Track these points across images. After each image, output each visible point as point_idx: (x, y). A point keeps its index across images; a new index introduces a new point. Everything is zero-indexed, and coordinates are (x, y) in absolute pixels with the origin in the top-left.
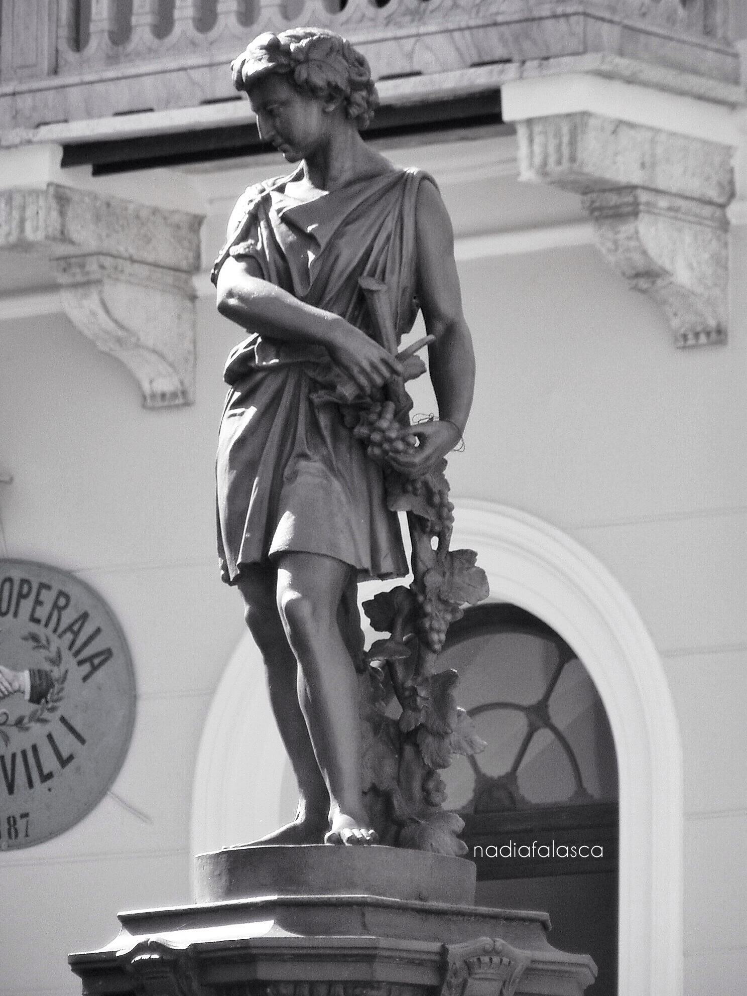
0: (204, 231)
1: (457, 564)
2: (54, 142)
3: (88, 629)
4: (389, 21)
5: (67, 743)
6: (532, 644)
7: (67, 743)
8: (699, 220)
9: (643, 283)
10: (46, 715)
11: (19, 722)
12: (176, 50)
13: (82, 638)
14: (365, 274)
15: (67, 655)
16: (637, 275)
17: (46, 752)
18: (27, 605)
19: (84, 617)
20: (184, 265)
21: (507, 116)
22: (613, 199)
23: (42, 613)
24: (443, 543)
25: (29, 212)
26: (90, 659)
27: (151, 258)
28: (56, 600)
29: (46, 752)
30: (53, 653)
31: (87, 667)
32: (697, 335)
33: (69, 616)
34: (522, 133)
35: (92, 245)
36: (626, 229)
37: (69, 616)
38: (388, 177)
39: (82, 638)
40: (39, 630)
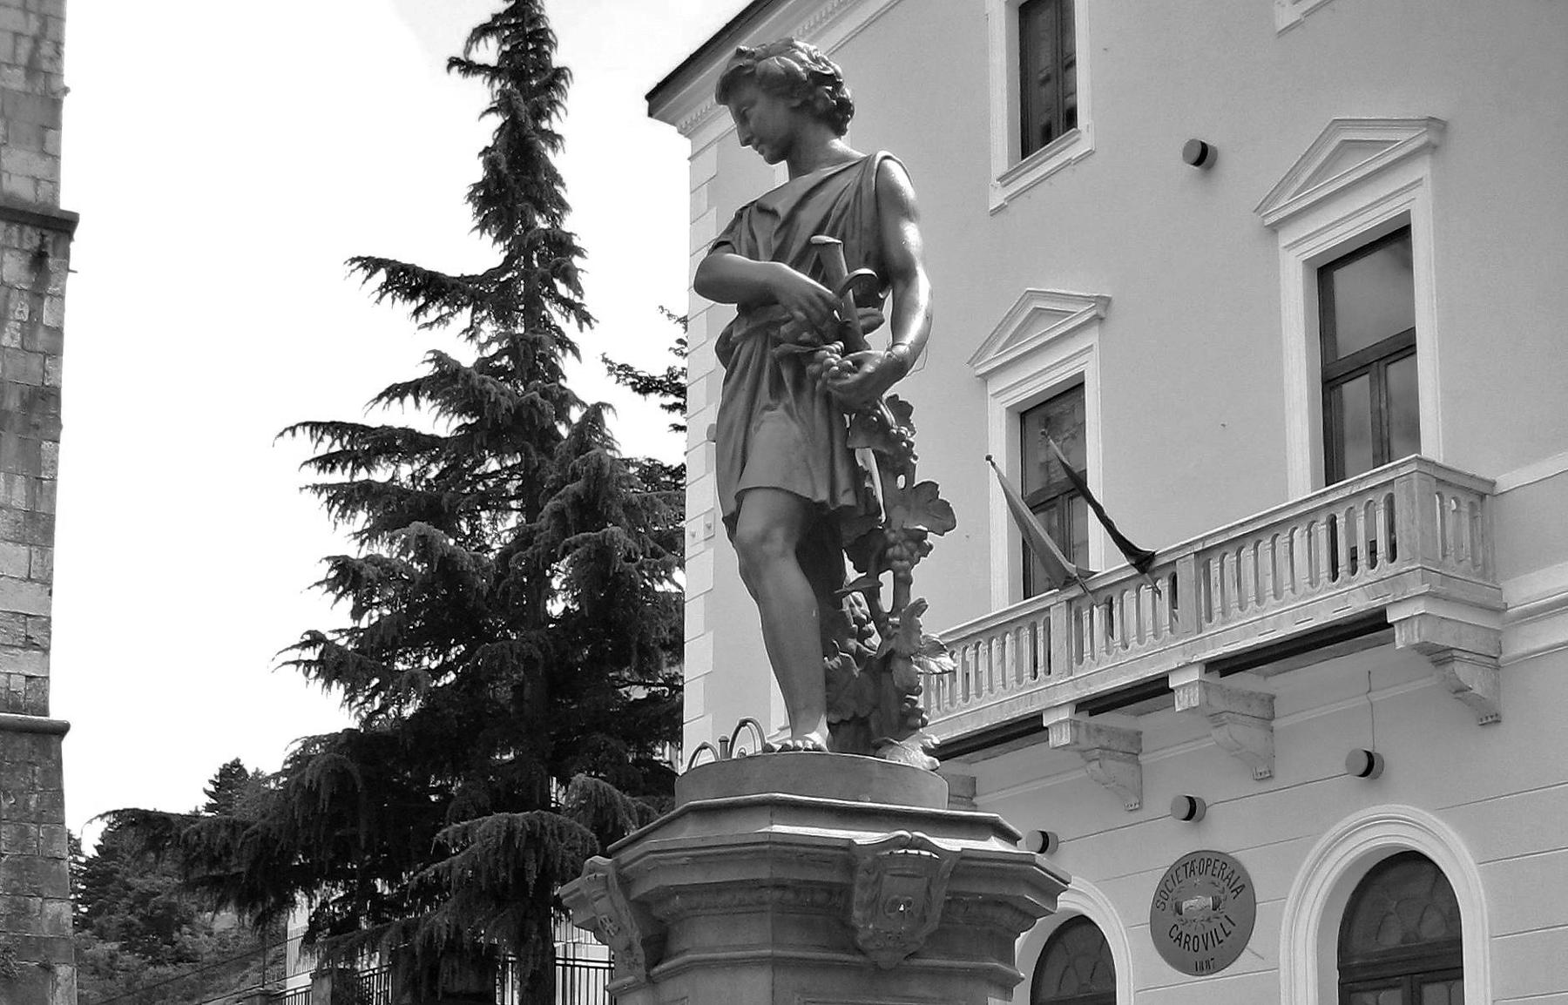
0: (1275, 701)
1: (1114, 767)
2: (1199, 662)
3: (1235, 877)
4: (1338, 587)
5: (1228, 927)
6: (1427, 867)
7: (1228, 927)
8: (1485, 665)
9: (1460, 695)
10: (1219, 915)
11: (1209, 919)
12: (1248, 615)
13: (1232, 881)
14: (577, 299)
15: (1227, 889)
16: (1457, 692)
17: (1220, 931)
18: (1211, 868)
19: (1233, 872)
20: (1266, 716)
21: (1045, 725)
22: (1442, 656)
23: (1216, 872)
24: (910, 480)
25: (1192, 694)
26: (1235, 890)
27: (1251, 714)
28: (678, 818)
29: (1220, 931)
30: (1221, 889)
31: (1235, 893)
32: (1487, 718)
33: (1227, 872)
34: (1396, 626)
35: (1223, 708)
36: (1449, 668)
37: (1227, 872)
38: (526, 119)
39: (1232, 881)
40: (1214, 879)
